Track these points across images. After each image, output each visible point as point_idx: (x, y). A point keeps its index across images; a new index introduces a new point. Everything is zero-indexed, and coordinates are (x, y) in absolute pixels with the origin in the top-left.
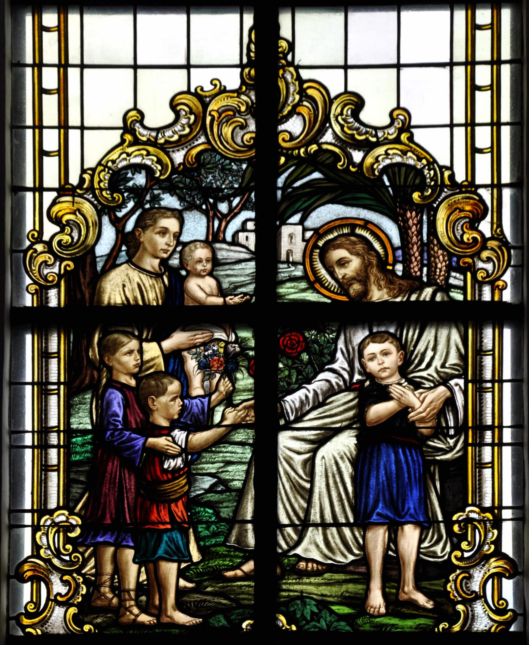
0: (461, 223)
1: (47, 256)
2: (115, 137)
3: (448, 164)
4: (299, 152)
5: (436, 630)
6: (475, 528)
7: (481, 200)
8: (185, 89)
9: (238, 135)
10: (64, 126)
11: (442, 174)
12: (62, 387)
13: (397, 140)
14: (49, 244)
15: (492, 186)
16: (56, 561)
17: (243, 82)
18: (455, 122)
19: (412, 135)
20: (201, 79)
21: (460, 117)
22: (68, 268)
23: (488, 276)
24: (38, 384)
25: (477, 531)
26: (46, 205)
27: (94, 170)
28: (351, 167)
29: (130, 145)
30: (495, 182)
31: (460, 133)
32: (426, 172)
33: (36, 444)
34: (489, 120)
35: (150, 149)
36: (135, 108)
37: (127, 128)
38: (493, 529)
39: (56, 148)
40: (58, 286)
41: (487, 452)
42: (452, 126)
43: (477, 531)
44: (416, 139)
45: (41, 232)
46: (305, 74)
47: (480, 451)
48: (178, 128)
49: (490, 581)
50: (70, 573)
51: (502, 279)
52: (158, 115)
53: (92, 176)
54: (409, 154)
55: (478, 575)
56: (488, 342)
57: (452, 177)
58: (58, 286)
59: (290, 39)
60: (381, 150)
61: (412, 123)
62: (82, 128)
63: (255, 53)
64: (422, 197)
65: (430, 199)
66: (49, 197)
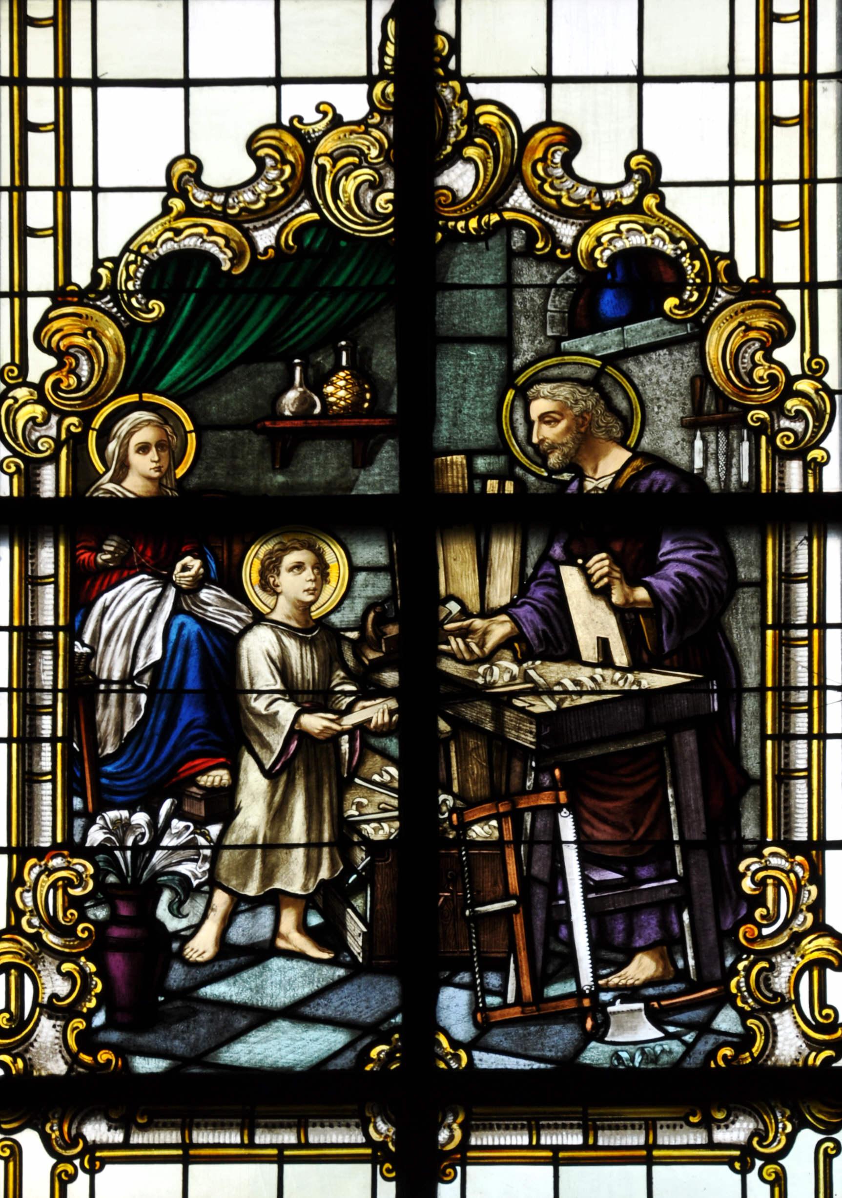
0: (750, 351)
1: (38, 410)
2: (153, 204)
3: (726, 249)
4: (456, 225)
5: (713, 1065)
6: (778, 883)
7: (783, 313)
8: (273, 120)
9: (361, 200)
10: (64, 187)
11: (714, 265)
12: (61, 635)
13: (636, 207)
14: (39, 387)
15: (800, 286)
16: (50, 938)
17: (373, 108)
18: (740, 70)
19: (662, 197)
20: (300, 103)
21: (746, 170)
22: (73, 429)
23: (797, 442)
24: (18, 629)
25: (782, 889)
26: (33, 321)
27: (116, 261)
28: (558, 252)
29: (180, 216)
30: (807, 279)
31: (746, 196)
32: (685, 261)
33: (15, 735)
34: (796, 176)
35: (219, 226)
36: (187, 155)
37: (174, 188)
38: (811, 884)
39: (50, 223)
40: (54, 459)
41: (800, 752)
42: (732, 183)
43: (782, 889)
44: (669, 206)
45: (24, 367)
46: (476, 91)
47: (787, 749)
48: (262, 186)
49: (806, 976)
50: (72, 958)
51: (822, 445)
52: (227, 165)
53: (114, 272)
54: (657, 231)
55: (786, 966)
56: (801, 565)
57: (732, 269)
58: (54, 459)
59: (452, 32)
60: (607, 226)
61: (664, 179)
62: (95, 189)
63: (395, 59)
64: (684, 305)
65: (699, 305)
66: (37, 308)
